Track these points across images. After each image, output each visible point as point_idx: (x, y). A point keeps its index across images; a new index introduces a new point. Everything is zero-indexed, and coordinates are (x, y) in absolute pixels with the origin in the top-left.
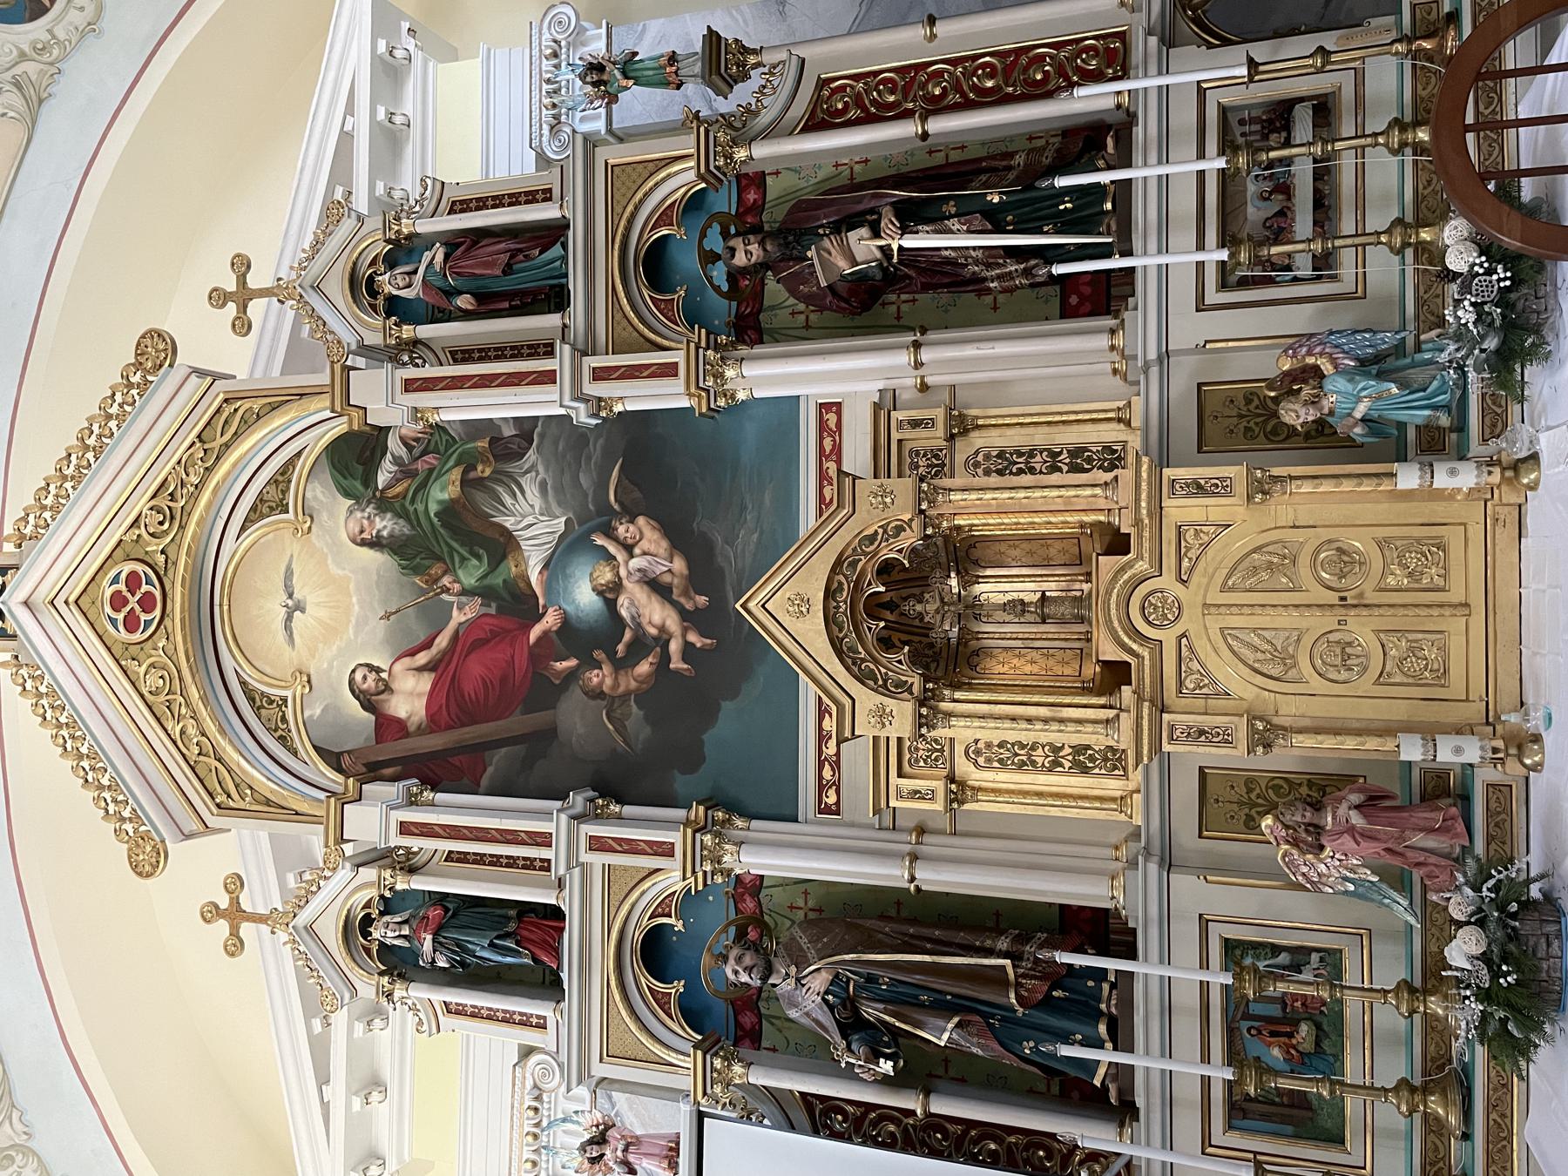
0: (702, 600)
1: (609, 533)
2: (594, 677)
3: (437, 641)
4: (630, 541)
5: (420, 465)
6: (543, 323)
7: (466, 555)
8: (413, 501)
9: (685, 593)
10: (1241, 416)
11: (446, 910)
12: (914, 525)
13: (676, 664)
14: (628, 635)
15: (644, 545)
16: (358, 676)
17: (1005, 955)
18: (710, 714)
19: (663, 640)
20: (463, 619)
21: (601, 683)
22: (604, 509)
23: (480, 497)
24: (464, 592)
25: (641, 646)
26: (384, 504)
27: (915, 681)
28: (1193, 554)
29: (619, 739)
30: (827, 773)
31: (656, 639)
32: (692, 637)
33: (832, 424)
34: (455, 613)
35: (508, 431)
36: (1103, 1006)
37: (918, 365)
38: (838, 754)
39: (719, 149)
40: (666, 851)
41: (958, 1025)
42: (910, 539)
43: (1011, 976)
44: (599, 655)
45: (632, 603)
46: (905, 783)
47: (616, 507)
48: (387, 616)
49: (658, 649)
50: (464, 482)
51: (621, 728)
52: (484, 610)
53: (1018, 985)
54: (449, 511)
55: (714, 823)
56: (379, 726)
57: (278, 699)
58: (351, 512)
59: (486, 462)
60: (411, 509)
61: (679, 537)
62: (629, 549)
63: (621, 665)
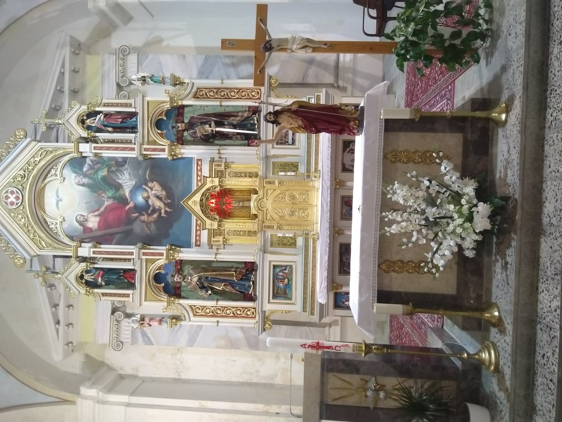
0: (169, 201)
1: (146, 185)
2: (143, 218)
3: (101, 209)
4: (152, 187)
5: (96, 167)
6: (130, 136)
7: (109, 189)
8: (94, 175)
9: (165, 199)
10: (280, 169)
11: (104, 272)
12: (218, 187)
13: (163, 215)
14: (151, 208)
15: (155, 188)
16: (78, 217)
17: (234, 271)
18: (171, 226)
19: (160, 210)
20: (108, 204)
21: (144, 219)
22: (145, 179)
23: (113, 176)
24: (109, 198)
25: (154, 211)
26: (85, 176)
27: (217, 217)
28: (269, 195)
29: (149, 232)
30: (198, 238)
31: (158, 209)
32: (167, 209)
33: (200, 164)
34: (106, 202)
35: (120, 160)
36: (252, 279)
37: (219, 153)
38: (200, 234)
39: (175, 102)
40: (162, 254)
41: (224, 285)
42: (218, 189)
43: (235, 275)
44: (144, 213)
45: (152, 201)
46: (214, 239)
47: (148, 179)
48: (86, 203)
49: (159, 212)
50: (108, 172)
51: (149, 229)
52: (114, 202)
53: (236, 277)
54: (104, 178)
55: (172, 249)
56: (84, 230)
57: (54, 223)
58: (76, 177)
59: (114, 167)
60: (93, 177)
61: (164, 186)
62: (152, 189)
63: (149, 215)
